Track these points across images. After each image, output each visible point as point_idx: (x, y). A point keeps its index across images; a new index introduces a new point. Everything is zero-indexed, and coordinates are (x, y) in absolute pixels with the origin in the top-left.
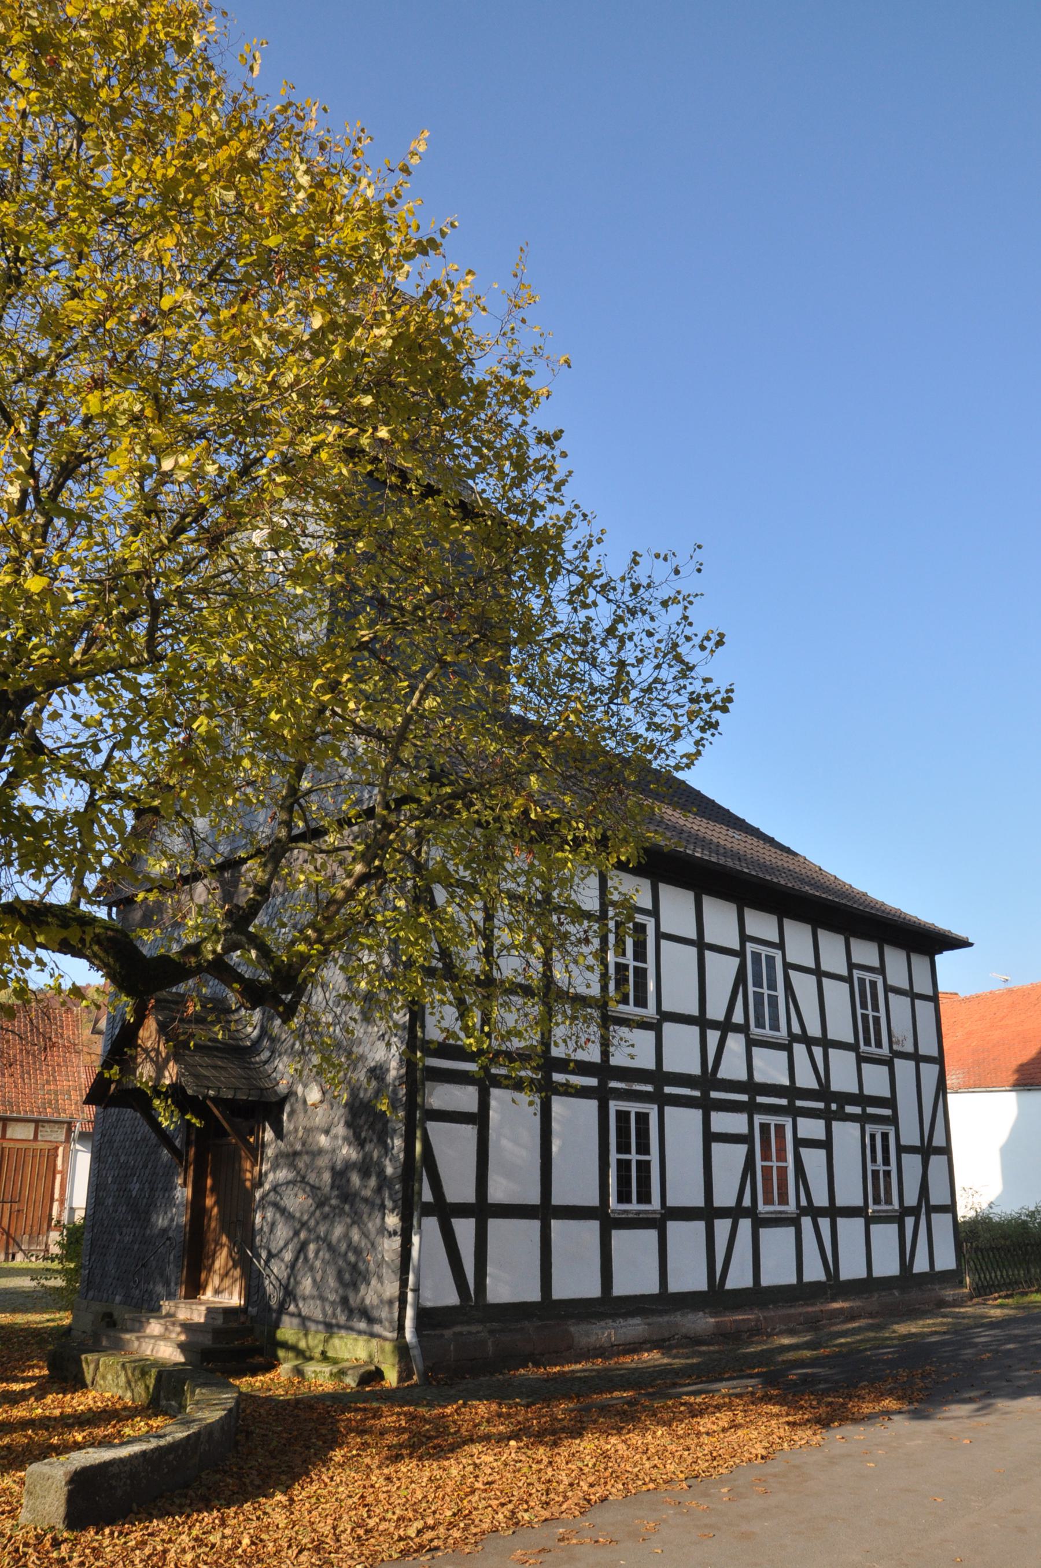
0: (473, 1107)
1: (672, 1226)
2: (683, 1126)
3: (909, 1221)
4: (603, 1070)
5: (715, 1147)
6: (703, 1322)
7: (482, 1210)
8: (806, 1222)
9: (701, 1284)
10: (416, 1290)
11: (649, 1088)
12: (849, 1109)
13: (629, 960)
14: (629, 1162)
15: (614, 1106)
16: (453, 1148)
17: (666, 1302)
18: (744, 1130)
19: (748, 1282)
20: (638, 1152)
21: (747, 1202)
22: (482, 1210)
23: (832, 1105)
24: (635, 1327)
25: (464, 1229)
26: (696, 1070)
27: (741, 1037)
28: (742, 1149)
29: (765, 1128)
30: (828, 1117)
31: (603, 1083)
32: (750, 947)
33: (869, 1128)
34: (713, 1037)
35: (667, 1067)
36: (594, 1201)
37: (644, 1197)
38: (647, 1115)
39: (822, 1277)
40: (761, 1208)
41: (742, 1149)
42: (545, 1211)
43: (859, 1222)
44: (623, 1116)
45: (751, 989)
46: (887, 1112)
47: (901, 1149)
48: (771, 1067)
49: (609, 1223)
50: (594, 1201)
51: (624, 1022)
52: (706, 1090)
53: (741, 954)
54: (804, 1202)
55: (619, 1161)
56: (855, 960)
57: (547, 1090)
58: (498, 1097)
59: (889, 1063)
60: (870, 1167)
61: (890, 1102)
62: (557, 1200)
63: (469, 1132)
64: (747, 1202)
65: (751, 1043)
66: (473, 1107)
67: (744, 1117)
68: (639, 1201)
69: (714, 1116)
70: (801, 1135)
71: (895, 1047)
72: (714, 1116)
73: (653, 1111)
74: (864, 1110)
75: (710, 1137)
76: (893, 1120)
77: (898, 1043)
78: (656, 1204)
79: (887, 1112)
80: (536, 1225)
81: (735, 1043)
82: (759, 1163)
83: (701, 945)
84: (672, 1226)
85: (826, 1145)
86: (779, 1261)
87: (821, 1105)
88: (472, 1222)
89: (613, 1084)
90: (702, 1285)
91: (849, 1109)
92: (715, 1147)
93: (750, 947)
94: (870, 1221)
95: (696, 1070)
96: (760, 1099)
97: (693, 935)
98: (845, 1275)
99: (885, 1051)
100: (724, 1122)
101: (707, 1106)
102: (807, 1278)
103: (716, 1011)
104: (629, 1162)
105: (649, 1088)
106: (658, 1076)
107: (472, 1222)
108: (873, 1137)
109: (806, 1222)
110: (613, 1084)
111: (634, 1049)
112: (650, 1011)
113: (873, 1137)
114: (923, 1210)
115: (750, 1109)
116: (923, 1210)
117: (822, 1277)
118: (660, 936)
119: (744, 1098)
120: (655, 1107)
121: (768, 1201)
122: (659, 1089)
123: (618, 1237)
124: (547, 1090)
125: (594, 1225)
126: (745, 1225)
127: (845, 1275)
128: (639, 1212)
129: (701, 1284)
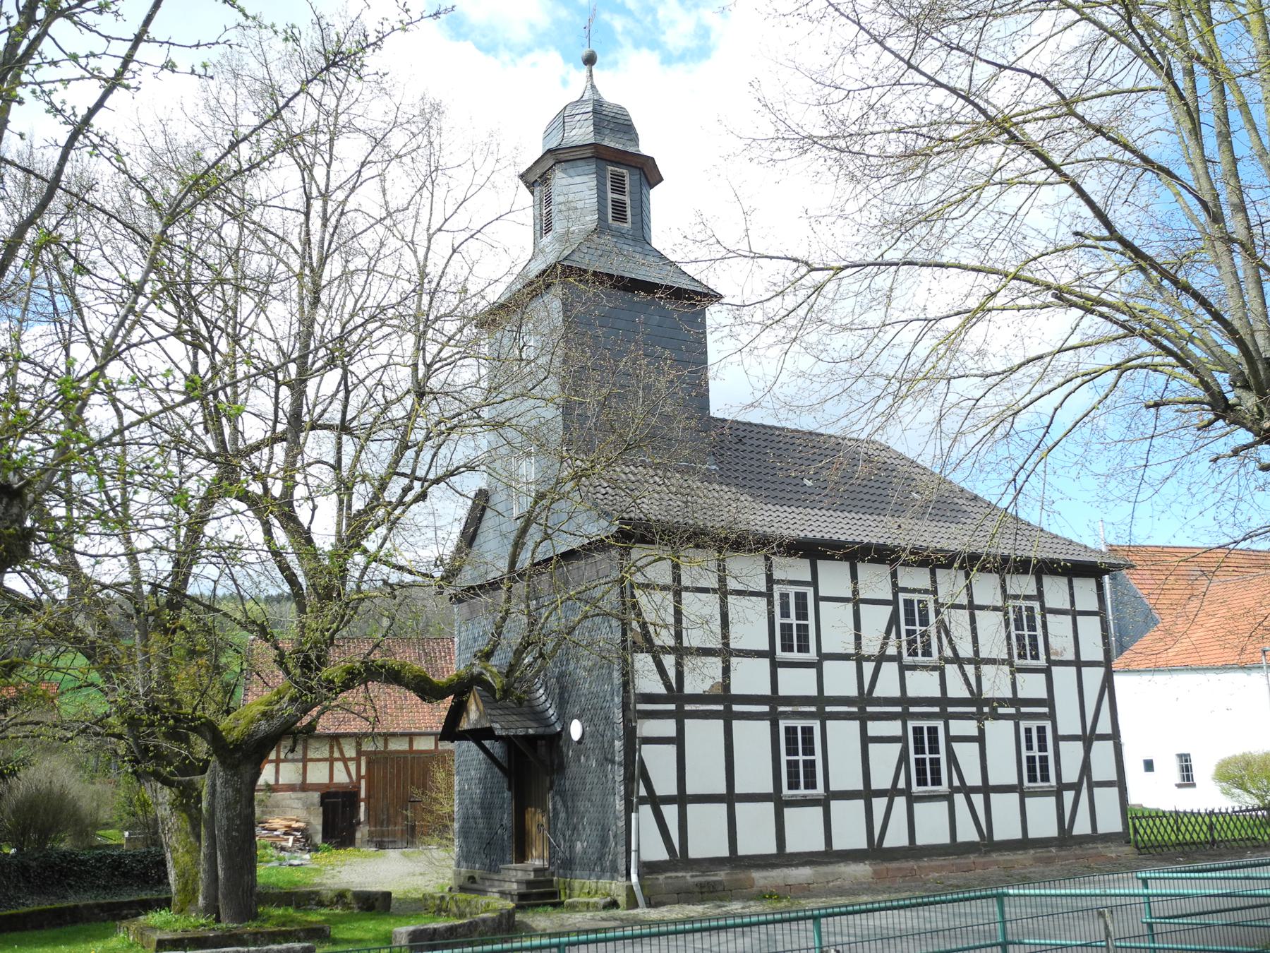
0: (975, 733)
1: (834, 804)
2: (842, 736)
3: (1069, 796)
4: (1015, 701)
5: (872, 747)
6: (862, 870)
7: (682, 799)
8: (959, 799)
9: (1052, 831)
10: (638, 851)
11: (813, 709)
12: (1001, 710)
13: (793, 620)
14: (797, 761)
15: (783, 724)
16: (659, 762)
17: (829, 856)
18: (899, 733)
19: (904, 842)
20: (804, 754)
21: (902, 784)
22: (986, 789)
23: (981, 707)
24: (803, 873)
25: (978, 799)
26: (853, 692)
27: (895, 666)
28: (897, 747)
29: (918, 731)
30: (980, 717)
31: (773, 709)
32: (902, 596)
33: (1023, 725)
34: (970, 669)
35: (828, 692)
36: (1015, 781)
37: (811, 784)
38: (1044, 728)
39: (975, 837)
40: (915, 788)
41: (897, 747)
42: (867, 794)
43: (1015, 797)
44: (791, 731)
45: (903, 627)
46: (1046, 710)
47: (1057, 738)
48: (923, 684)
49: (1024, 795)
50: (1015, 781)
51: (913, 668)
52: (863, 706)
53: (894, 603)
54: (956, 783)
55: (789, 762)
56: (1010, 591)
57: (728, 718)
58: (989, 725)
59: (1047, 672)
60: (1025, 753)
61: (1049, 702)
62: (992, 782)
63: (672, 749)
64: (902, 784)
65: (903, 669)
66: (975, 733)
67: (898, 724)
68: (806, 787)
69: (870, 724)
70: (952, 733)
71: (1053, 658)
72: (870, 724)
73: (816, 725)
74: (1018, 710)
75: (866, 740)
76: (1052, 716)
77: (1057, 654)
78: (820, 789)
79: (1046, 710)
80: (724, 807)
81: (890, 669)
82: (913, 757)
83: (972, 607)
84: (834, 804)
85: (980, 739)
86: (932, 824)
87: (974, 709)
88: (675, 807)
89: (781, 709)
90: (863, 844)
91: (1001, 710)
92: (871, 746)
93: (1010, 602)
94: (1024, 795)
95: (853, 692)
96: (912, 709)
97: (1067, 606)
98: (998, 836)
99: (1042, 662)
100: (875, 728)
101: (864, 718)
102: (960, 839)
103: (871, 647)
104: (797, 761)
105: (813, 709)
106: (820, 700)
107: (675, 807)
108: (1028, 731)
109: (959, 799)
110: (781, 709)
111: (797, 683)
112: (812, 655)
113: (1028, 731)
114: (1085, 785)
115: (904, 717)
116: (1085, 785)
117: (975, 837)
118: (818, 599)
119: (899, 709)
120: (818, 722)
121: (921, 782)
122: (943, 710)
123: (918, 807)
124: (728, 718)
125: (770, 807)
126: (900, 803)
127: (998, 836)
128: (805, 796)
129: (1052, 831)
